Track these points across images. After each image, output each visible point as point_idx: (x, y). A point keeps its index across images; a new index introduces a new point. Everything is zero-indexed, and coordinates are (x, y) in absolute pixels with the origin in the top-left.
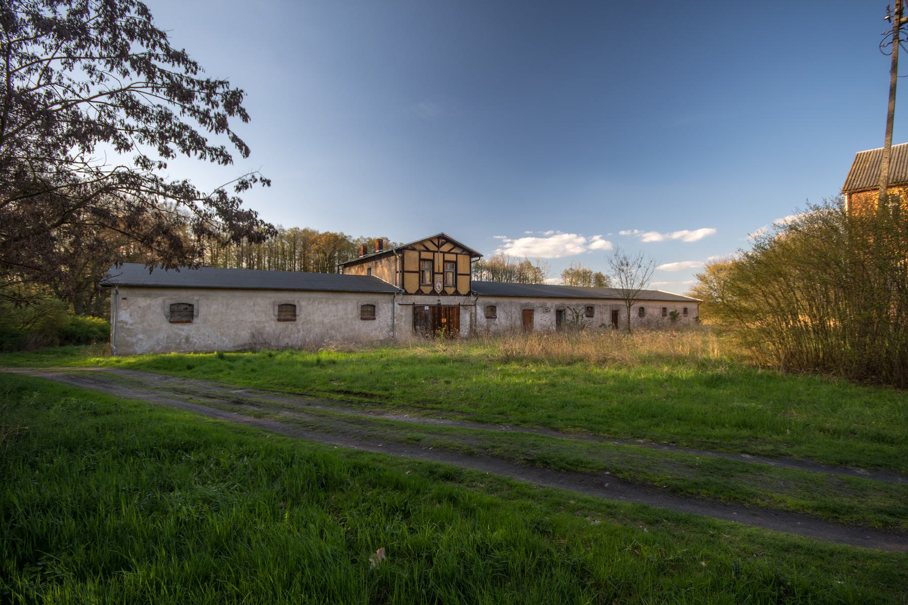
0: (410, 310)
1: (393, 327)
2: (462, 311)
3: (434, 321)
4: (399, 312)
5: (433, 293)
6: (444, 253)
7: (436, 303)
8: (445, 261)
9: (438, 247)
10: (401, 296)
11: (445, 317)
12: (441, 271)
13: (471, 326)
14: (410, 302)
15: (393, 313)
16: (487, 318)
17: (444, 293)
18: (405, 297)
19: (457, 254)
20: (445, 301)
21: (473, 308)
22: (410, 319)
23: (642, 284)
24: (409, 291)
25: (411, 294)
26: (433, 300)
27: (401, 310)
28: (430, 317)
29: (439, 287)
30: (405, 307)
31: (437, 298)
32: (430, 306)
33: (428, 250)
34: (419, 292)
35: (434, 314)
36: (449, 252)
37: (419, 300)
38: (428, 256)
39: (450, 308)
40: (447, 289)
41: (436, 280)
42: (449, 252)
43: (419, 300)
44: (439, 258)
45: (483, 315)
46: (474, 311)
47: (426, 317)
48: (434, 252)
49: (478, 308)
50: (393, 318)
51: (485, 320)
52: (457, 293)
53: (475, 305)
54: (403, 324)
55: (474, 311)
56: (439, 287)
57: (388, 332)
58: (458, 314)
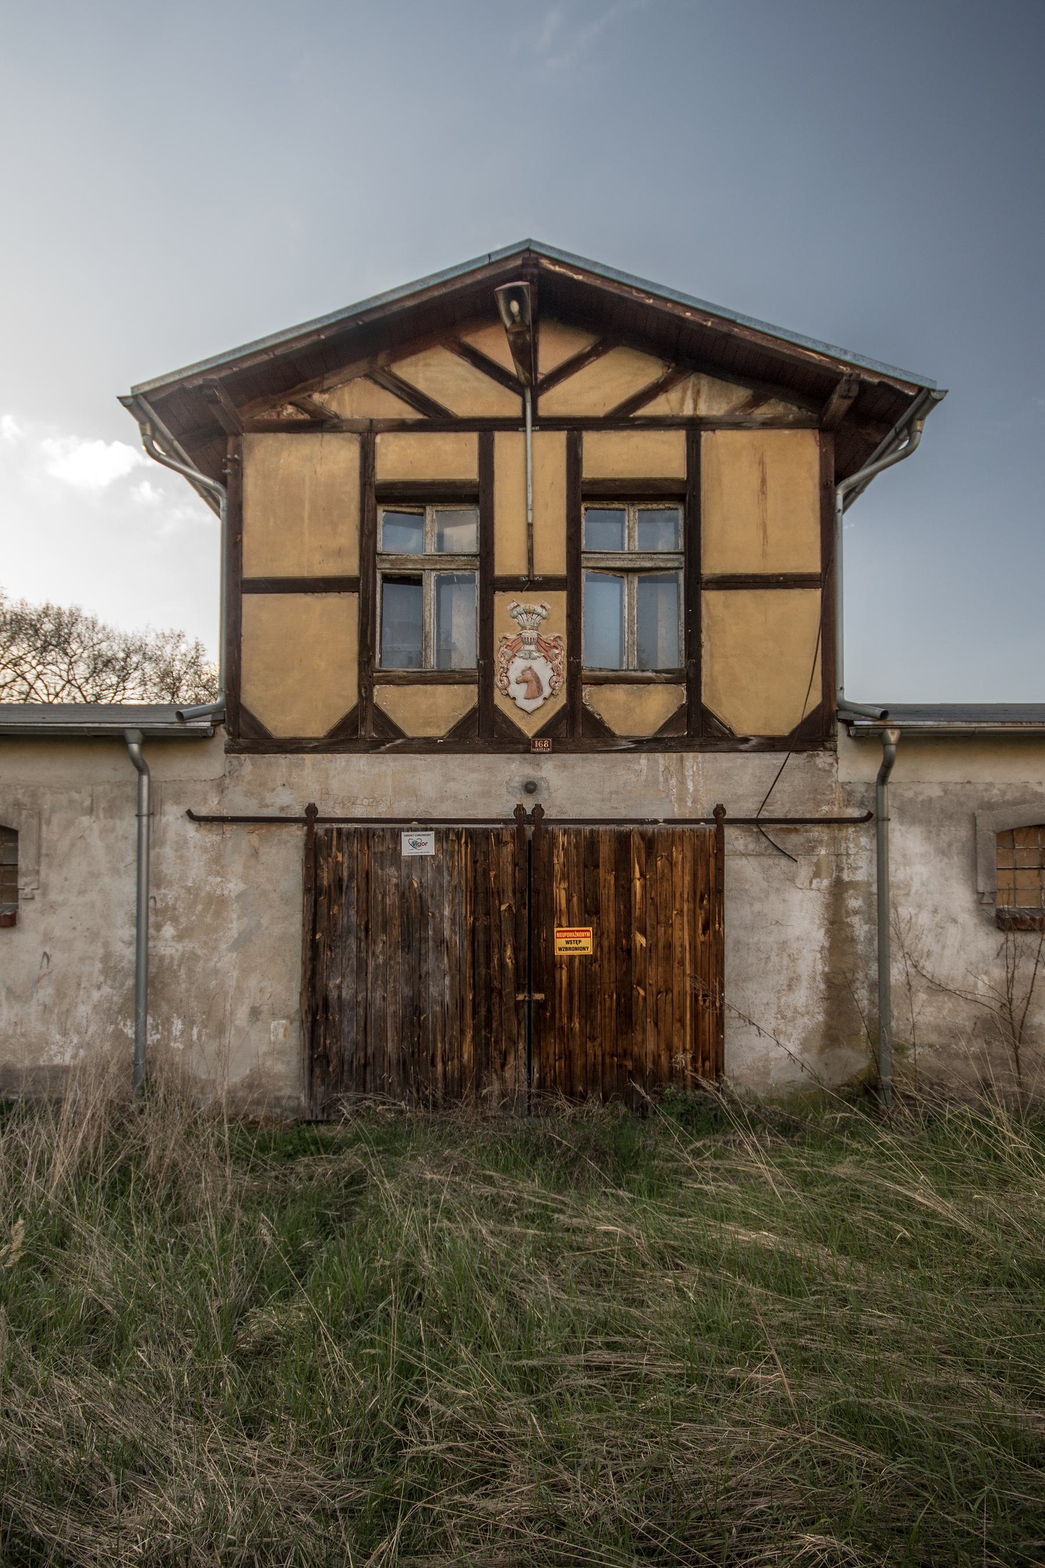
0: (284, 858)
1: (146, 987)
2: (744, 865)
3: (481, 940)
4: (197, 869)
5: (485, 730)
6: (575, 427)
7: (501, 805)
8: (587, 494)
9: (529, 384)
10: (213, 763)
11: (590, 912)
12: (552, 561)
13: (837, 990)
14: (285, 800)
15: (765, 536)
16: (1005, 923)
17: (576, 729)
18: (248, 764)
19: (694, 428)
20: (578, 789)
21: (859, 846)
22: (284, 924)
23: (390, 806)
24: (279, 724)
25: (294, 746)
26: (480, 788)
27: (217, 863)
28: (448, 916)
29: (529, 681)
30: (245, 838)
31: (513, 769)
32: (447, 831)
33: (434, 418)
34: (363, 730)
35: (480, 893)
36: (622, 418)
37: (356, 785)
38: (450, 457)
39: (622, 848)
40: (608, 704)
41: (504, 630)
42: (622, 418)
43: (356, 785)
44: (530, 478)
45: (960, 898)
46: (861, 869)
47: (414, 916)
48: (486, 428)
49: (907, 842)
50: (144, 918)
51: (986, 942)
52: (697, 728)
53: (873, 820)
54: (226, 960)
55: (861, 869)
56: (529, 681)
57: (109, 1014)
58: (710, 893)
